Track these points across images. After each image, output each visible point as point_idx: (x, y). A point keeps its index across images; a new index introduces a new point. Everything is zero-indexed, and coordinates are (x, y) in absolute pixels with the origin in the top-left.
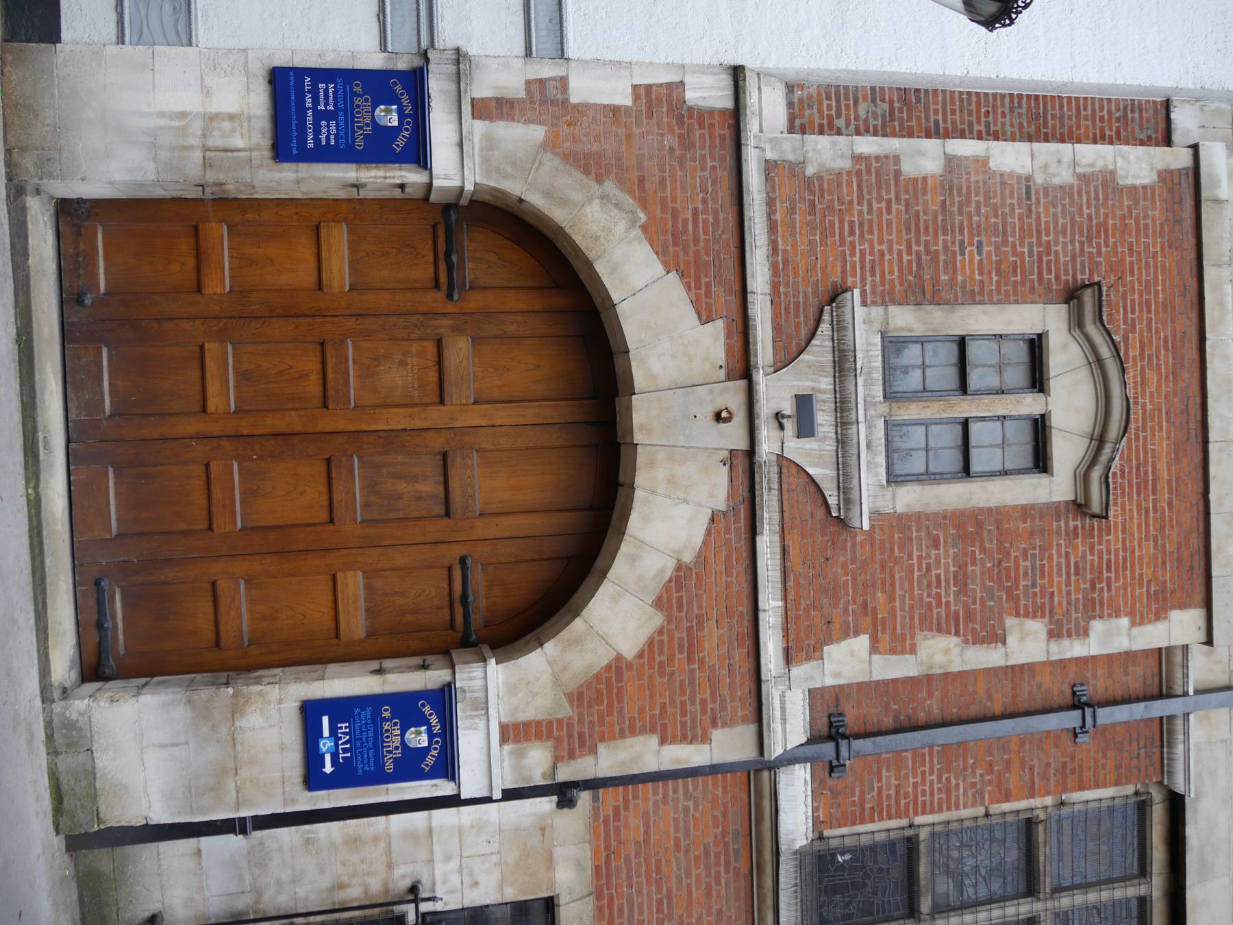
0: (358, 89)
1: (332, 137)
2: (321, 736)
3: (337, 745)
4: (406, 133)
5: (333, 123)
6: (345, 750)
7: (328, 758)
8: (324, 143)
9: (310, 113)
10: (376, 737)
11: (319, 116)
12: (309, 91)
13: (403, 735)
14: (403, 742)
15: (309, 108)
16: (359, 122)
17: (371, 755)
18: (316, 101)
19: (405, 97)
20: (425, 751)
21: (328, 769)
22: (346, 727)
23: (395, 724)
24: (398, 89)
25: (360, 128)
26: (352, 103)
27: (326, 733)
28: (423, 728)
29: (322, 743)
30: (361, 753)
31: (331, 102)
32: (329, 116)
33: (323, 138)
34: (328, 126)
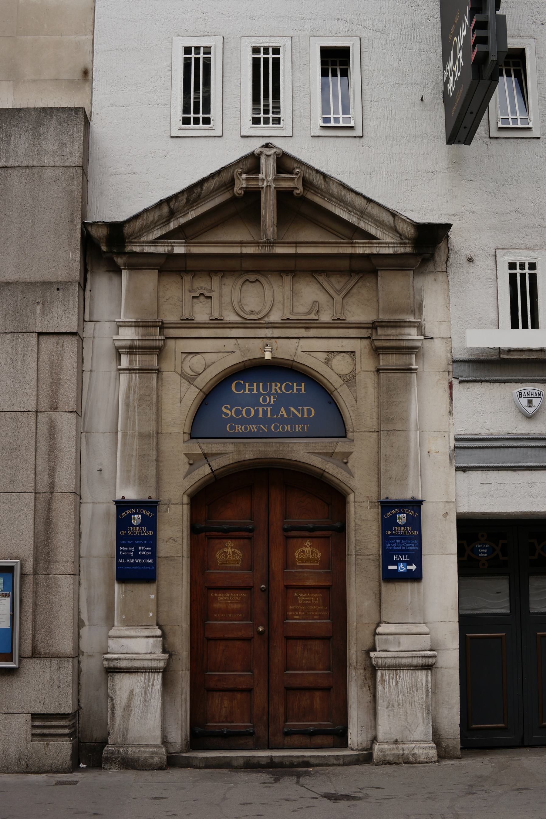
0: (389, 533)
1: (147, 549)
2: (397, 570)
3: (403, 562)
4: (144, 512)
5: (140, 548)
6: (405, 558)
7: (409, 567)
8: (150, 553)
9: (137, 561)
11: (137, 556)
12: (126, 560)
13: (400, 526)
14: (139, 526)
15: (135, 561)
16: (405, 533)
18: (130, 557)
19: (392, 512)
20: (407, 515)
21: (413, 567)
22: (396, 557)
23: (395, 529)
26: (395, 535)
27: (395, 567)
30: (408, 547)
31: (130, 549)
33: (148, 553)
34: (142, 550)
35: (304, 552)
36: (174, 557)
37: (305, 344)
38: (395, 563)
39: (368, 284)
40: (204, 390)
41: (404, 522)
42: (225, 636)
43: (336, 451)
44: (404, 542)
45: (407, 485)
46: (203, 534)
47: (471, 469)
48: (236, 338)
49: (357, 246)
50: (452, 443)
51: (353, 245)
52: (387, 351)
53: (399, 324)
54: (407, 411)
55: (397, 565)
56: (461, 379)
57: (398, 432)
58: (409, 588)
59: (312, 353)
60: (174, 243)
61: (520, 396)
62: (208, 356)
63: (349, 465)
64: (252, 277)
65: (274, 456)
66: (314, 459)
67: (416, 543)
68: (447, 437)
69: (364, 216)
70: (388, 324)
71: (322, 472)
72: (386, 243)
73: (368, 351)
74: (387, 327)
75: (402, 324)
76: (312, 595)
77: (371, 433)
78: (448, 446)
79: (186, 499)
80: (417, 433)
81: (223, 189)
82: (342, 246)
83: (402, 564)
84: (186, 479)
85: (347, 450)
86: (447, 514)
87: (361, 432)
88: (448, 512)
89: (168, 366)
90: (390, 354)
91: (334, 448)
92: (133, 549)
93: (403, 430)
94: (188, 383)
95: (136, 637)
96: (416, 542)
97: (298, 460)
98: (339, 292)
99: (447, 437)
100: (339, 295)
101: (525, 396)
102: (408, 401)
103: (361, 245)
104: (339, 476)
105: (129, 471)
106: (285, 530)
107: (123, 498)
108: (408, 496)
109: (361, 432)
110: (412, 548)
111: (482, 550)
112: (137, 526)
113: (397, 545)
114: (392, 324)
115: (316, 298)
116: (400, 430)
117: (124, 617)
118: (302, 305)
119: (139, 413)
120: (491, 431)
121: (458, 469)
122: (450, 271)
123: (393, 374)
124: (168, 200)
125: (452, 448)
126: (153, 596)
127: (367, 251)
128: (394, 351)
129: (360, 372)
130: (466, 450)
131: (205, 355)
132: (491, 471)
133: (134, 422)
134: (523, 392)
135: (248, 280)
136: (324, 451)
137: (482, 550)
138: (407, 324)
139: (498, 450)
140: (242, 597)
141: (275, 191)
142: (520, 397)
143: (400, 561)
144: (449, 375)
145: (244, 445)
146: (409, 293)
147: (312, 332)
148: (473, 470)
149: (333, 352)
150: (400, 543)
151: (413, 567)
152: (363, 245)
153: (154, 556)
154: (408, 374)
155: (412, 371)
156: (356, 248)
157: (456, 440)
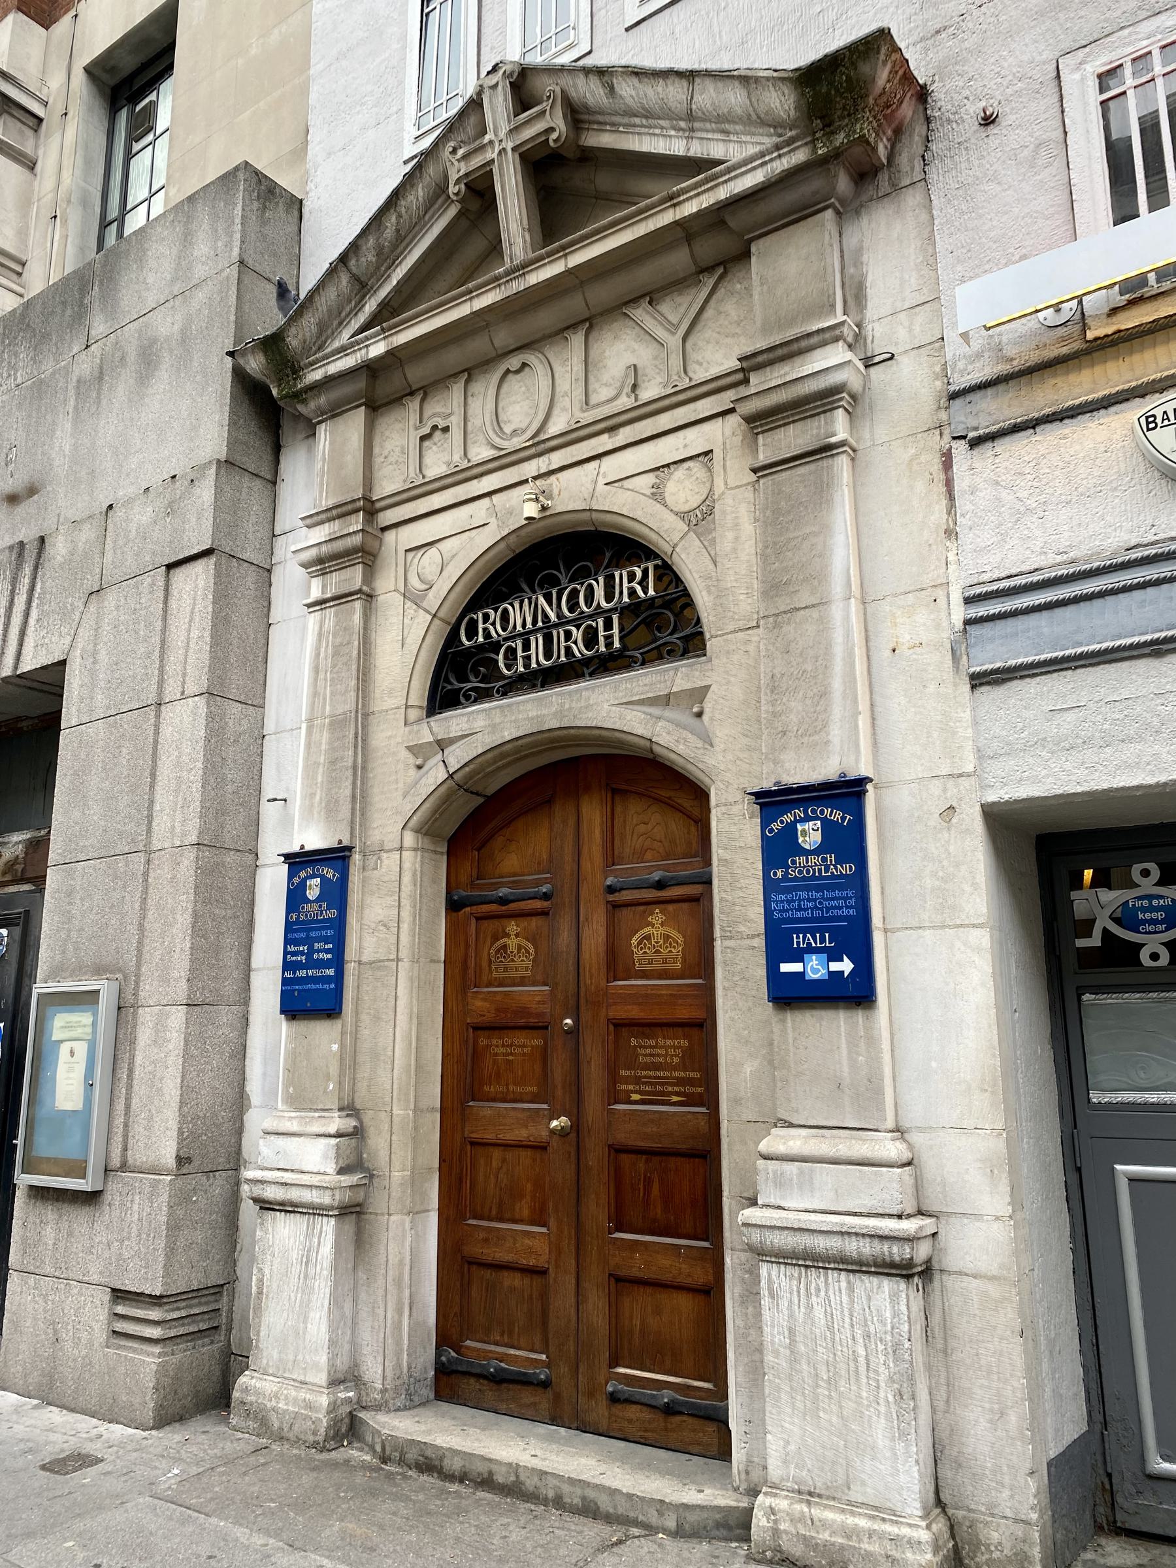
0: (780, 873)
2: (802, 974)
3: (817, 951)
6: (823, 940)
7: (835, 966)
9: (310, 973)
10: (808, 888)
13: (807, 853)
16: (820, 870)
17: (831, 894)
21: (845, 966)
22: (798, 937)
23: (794, 862)
24: (777, 826)
25: (827, 869)
26: (795, 879)
27: (796, 967)
28: (799, 827)
29: (811, 975)
30: (828, 909)
31: (301, 948)
32: (312, 951)
34: (319, 951)
35: (648, 938)
36: (383, 961)
37: (613, 466)
38: (798, 956)
39: (738, 286)
40: (441, 614)
41: (815, 842)
42: (500, 1136)
43: (675, 690)
44: (818, 895)
45: (827, 743)
46: (468, 909)
47: (1018, 674)
48: (489, 494)
49: (684, 201)
50: (959, 613)
51: (675, 201)
52: (773, 422)
53: (795, 347)
54: (824, 555)
55: (801, 960)
56: (972, 435)
57: (802, 612)
58: (861, 1020)
59: (626, 483)
60: (367, 339)
61: (1152, 425)
62: (445, 546)
63: (705, 717)
64: (514, 362)
65: (554, 724)
66: (628, 718)
67: (851, 898)
68: (942, 601)
69: (697, 125)
70: (771, 356)
71: (648, 744)
72: (745, 162)
73: (741, 438)
74: (771, 363)
75: (804, 344)
76: (669, 1042)
77: (750, 632)
78: (945, 624)
79: (409, 839)
80: (849, 605)
81: (440, 201)
82: (652, 215)
83: (814, 957)
84: (409, 798)
85: (699, 684)
86: (951, 811)
87: (727, 633)
88: (954, 805)
89: (387, 584)
90: (780, 426)
91: (669, 683)
92: (305, 948)
93: (813, 606)
94: (415, 607)
95: (299, 1135)
96: (850, 894)
97: (599, 725)
98: (672, 328)
99: (942, 601)
100: (673, 334)
101: (1166, 422)
102: (825, 529)
103: (692, 193)
104: (681, 749)
105: (313, 795)
106: (611, 890)
107: (302, 847)
108: (825, 770)
109: (727, 633)
110: (840, 913)
111: (1148, 916)
112: (313, 902)
113: (799, 905)
114: (780, 352)
115: (630, 359)
116: (806, 607)
117: (291, 1090)
118: (606, 385)
119: (332, 680)
120: (1071, 554)
121: (979, 680)
122: (933, 176)
123: (788, 473)
124: (343, 259)
125: (959, 625)
126: (335, 1047)
127: (706, 201)
128: (788, 417)
129: (723, 493)
130: (1000, 624)
131: (439, 545)
132: (1079, 671)
133: (325, 699)
134: (1159, 413)
135: (508, 371)
136: (650, 695)
137: (1148, 916)
138: (814, 340)
139: (1097, 603)
140: (532, 1047)
141: (517, 156)
142: (1148, 430)
143: (811, 950)
144: (941, 434)
145: (503, 712)
146: (824, 268)
147: (625, 435)
148: (1022, 677)
149: (668, 466)
150: (809, 900)
151: (845, 966)
152: (695, 192)
153: (339, 962)
154: (825, 463)
155: (834, 452)
156: (682, 206)
157: (969, 601)
